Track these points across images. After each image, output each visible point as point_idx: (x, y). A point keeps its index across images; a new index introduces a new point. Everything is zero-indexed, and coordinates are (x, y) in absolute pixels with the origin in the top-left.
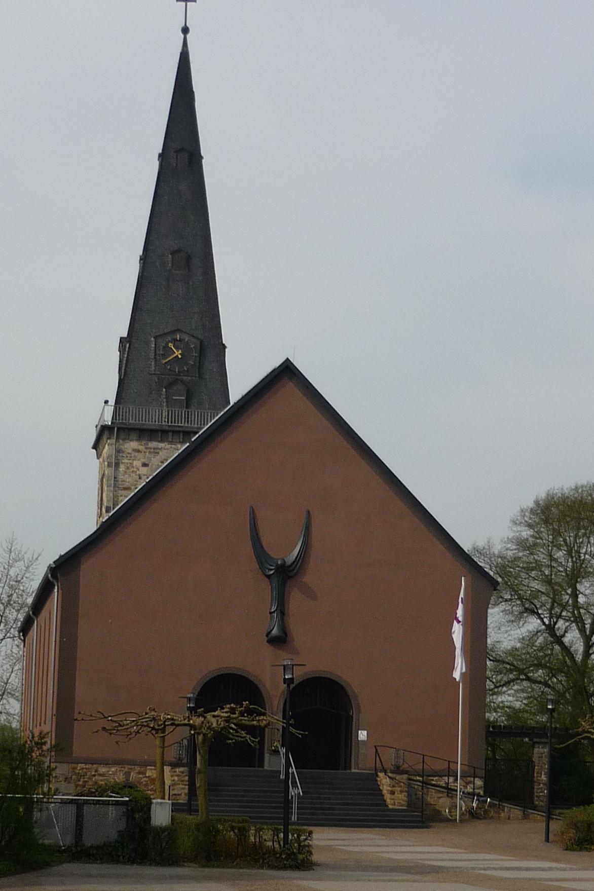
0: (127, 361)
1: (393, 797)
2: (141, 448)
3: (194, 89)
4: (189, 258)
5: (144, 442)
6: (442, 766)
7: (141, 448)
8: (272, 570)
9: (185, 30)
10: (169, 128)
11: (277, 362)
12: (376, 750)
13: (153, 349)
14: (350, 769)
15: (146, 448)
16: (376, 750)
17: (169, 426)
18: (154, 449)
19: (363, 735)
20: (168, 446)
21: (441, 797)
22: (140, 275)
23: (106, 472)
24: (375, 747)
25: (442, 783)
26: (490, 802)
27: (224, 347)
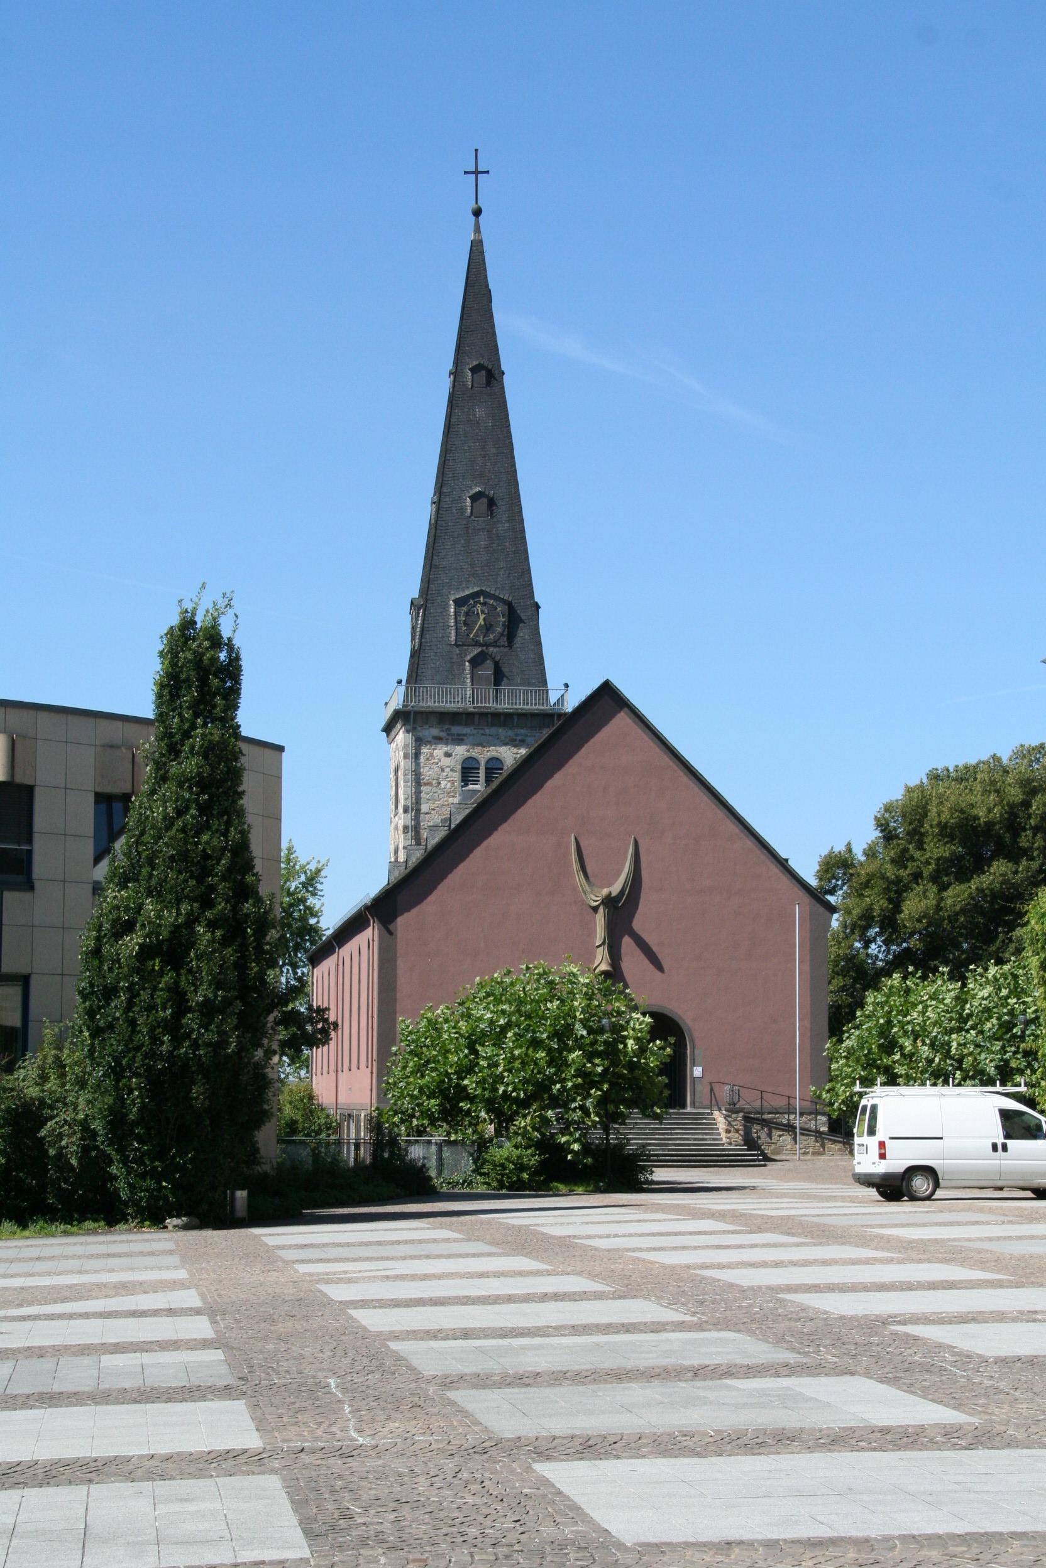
0: (422, 632)
1: (729, 1135)
2: (443, 734)
3: (492, 286)
4: (492, 503)
5: (446, 727)
6: (780, 1103)
7: (443, 734)
8: (596, 901)
9: (477, 213)
10: (450, 456)
11: (596, 685)
12: (712, 1090)
13: (452, 614)
14: (684, 1106)
15: (448, 735)
16: (712, 1090)
17: (474, 708)
18: (458, 735)
19: (698, 1071)
20: (475, 732)
21: (782, 1135)
22: (433, 522)
23: (402, 764)
24: (711, 1083)
25: (785, 1122)
26: (843, 966)
27: (537, 607)
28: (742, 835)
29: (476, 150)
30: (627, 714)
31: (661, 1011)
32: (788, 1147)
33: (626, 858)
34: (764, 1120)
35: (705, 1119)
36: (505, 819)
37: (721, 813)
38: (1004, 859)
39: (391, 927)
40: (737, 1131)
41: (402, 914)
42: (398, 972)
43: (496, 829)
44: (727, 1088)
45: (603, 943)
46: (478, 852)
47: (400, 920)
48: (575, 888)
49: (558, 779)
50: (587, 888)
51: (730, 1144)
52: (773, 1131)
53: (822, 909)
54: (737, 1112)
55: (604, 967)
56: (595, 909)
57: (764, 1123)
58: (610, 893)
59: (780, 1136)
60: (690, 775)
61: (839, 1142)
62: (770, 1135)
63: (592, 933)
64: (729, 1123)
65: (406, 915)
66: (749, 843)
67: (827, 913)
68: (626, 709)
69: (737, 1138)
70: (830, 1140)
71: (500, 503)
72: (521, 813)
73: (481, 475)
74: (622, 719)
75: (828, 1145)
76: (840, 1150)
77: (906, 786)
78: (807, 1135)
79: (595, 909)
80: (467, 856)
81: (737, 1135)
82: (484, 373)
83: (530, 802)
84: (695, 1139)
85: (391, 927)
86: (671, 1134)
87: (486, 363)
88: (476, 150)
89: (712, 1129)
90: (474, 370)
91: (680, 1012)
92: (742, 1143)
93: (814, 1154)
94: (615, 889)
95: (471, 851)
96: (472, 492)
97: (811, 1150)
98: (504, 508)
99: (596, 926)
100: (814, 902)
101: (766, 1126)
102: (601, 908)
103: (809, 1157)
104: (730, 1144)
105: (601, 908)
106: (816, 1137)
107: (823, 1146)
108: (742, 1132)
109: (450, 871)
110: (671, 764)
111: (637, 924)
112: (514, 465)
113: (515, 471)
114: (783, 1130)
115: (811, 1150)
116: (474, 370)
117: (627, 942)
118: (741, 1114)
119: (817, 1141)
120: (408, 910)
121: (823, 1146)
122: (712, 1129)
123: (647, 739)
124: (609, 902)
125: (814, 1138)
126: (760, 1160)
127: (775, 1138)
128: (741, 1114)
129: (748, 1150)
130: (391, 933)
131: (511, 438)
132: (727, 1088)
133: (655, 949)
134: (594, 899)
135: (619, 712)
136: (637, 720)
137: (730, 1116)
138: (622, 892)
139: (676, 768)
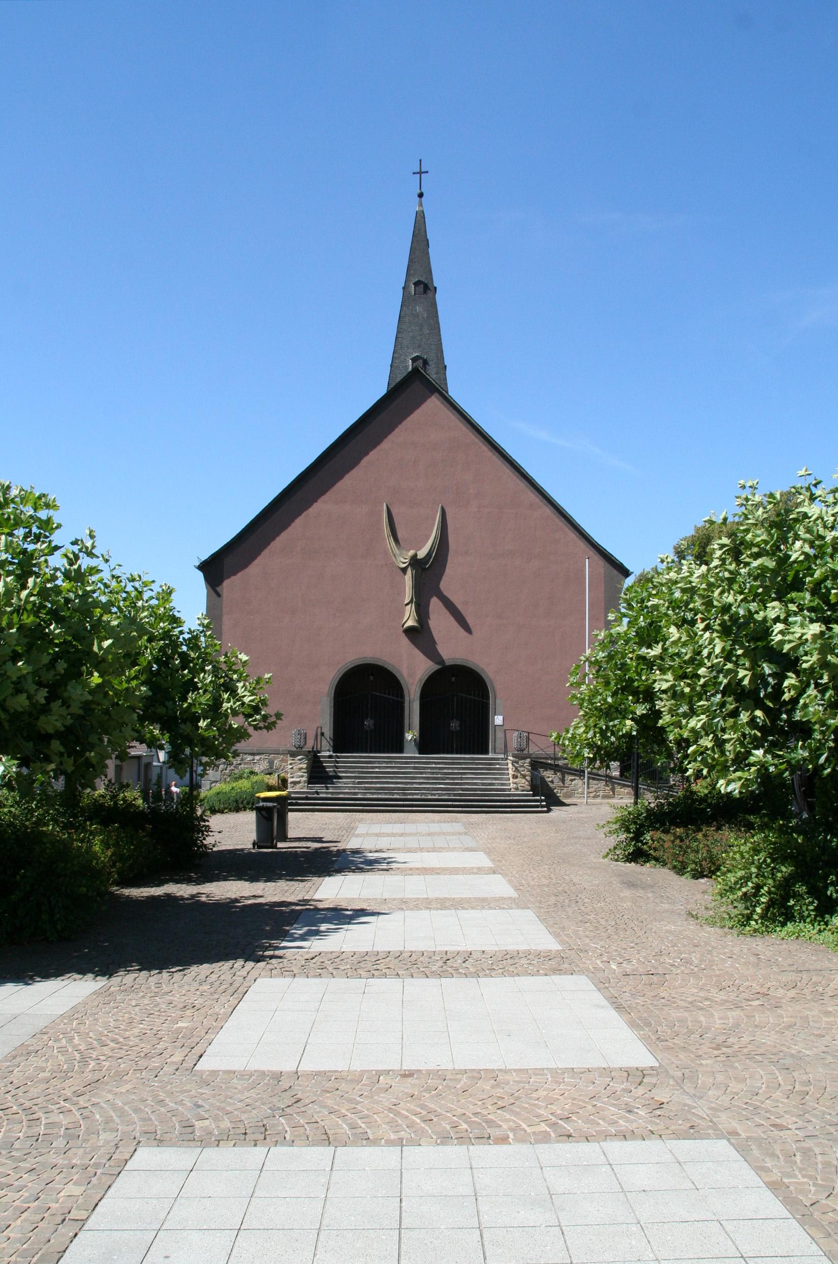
1: (515, 780)
19: (498, 720)
21: (574, 779)
28: (541, 504)
29: (420, 160)
30: (437, 398)
31: (465, 664)
32: (580, 790)
33: (434, 524)
34: (557, 766)
35: (498, 764)
36: (323, 492)
37: (522, 485)
38: (709, 825)
39: (218, 589)
40: (524, 776)
41: (229, 577)
42: (223, 627)
43: (316, 501)
44: (516, 734)
45: (411, 602)
46: (299, 521)
47: (226, 583)
48: (386, 552)
49: (373, 455)
50: (397, 551)
51: (517, 789)
52: (566, 776)
53: (615, 572)
54: (524, 758)
55: (411, 623)
56: (404, 570)
57: (556, 768)
58: (416, 555)
59: (572, 780)
60: (494, 451)
61: (628, 786)
62: (563, 780)
63: (402, 593)
64: (516, 768)
65: (233, 578)
66: (548, 511)
67: (621, 576)
68: (436, 394)
69: (524, 783)
70: (619, 784)
71: (430, 363)
72: (340, 485)
73: (419, 346)
74: (433, 403)
75: (618, 789)
76: (628, 793)
77: (695, 526)
78: (598, 780)
79: (404, 570)
80: (289, 525)
81: (524, 781)
82: (422, 286)
83: (347, 477)
84: (483, 784)
85: (218, 589)
86: (461, 779)
87: (423, 279)
88: (420, 160)
89: (503, 774)
90: (416, 284)
91: (482, 666)
92: (529, 788)
93: (604, 797)
94: (422, 554)
95: (293, 521)
96: (413, 356)
97: (601, 793)
98: (433, 366)
99: (405, 586)
100: (608, 565)
101: (559, 771)
102: (409, 571)
103: (598, 800)
104: (517, 789)
105: (409, 571)
106: (606, 781)
107: (613, 790)
108: (528, 778)
109: (274, 539)
110: (476, 440)
111: (444, 585)
112: (440, 340)
113: (441, 344)
114: (575, 775)
115: (601, 793)
116: (416, 284)
117: (435, 604)
118: (528, 760)
119: (607, 786)
120: (235, 574)
121: (613, 790)
122: (503, 774)
123: (453, 418)
124: (415, 562)
125: (604, 783)
126: (542, 806)
127: (567, 782)
128: (528, 760)
129: (534, 795)
130: (219, 595)
131: (439, 324)
132: (516, 734)
133: (460, 607)
134: (403, 560)
135: (430, 397)
136: (445, 403)
137: (517, 763)
138: (429, 554)
139: (481, 444)
